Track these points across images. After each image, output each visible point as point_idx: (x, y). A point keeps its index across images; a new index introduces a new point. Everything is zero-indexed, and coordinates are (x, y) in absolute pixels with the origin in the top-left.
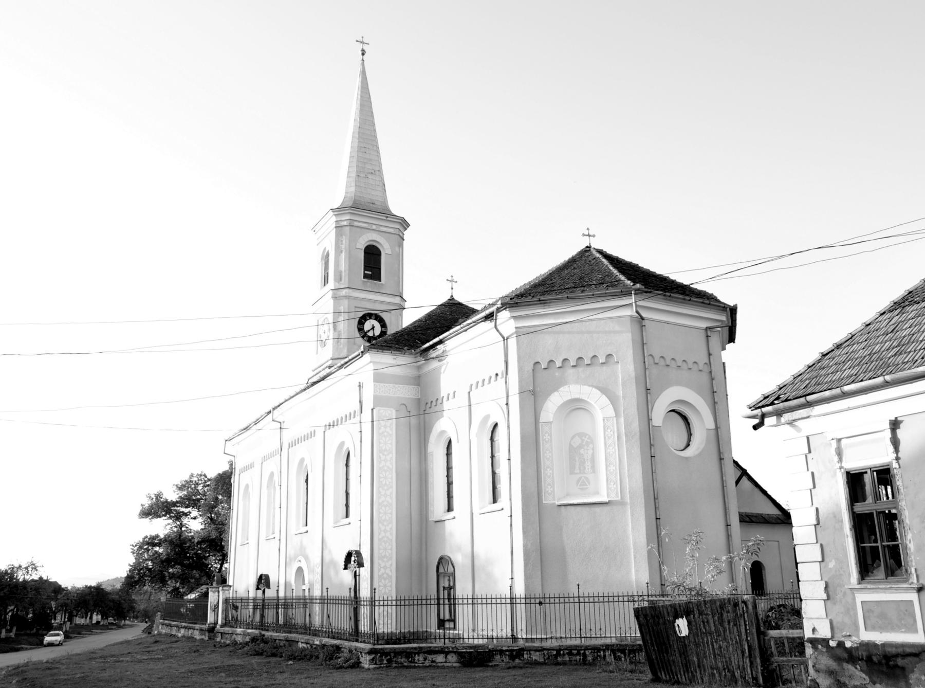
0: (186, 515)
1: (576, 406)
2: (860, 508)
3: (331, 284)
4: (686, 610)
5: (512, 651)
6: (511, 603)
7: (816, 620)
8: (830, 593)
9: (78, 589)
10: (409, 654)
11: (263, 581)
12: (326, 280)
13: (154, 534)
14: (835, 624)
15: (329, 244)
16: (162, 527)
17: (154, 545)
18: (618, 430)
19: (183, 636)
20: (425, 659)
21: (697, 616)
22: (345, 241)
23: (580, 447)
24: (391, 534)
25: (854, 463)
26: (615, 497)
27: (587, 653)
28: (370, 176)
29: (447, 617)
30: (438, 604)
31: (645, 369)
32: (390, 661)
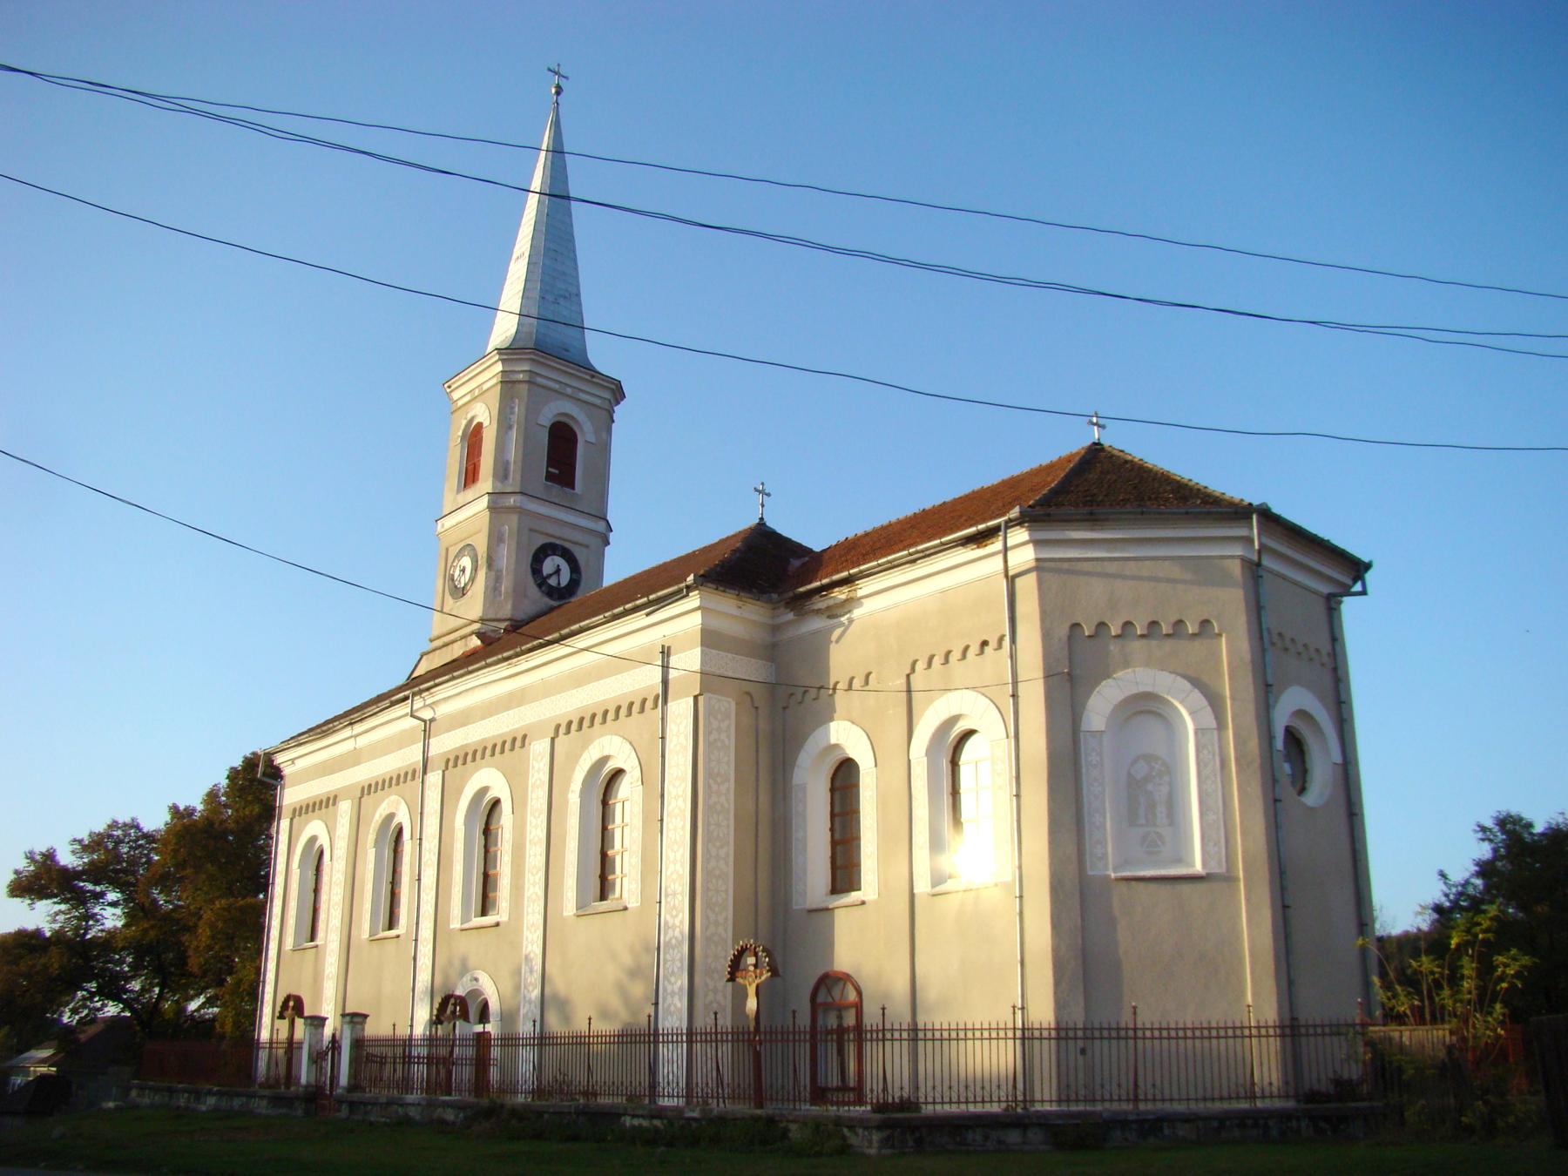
11: (451, 1007)
16: (42, 916)
20: (986, 1138)
22: (518, 409)
23: (1148, 778)
26: (1218, 868)
27: (1271, 1123)
28: (561, 301)
29: (834, 1081)
32: (919, 1142)
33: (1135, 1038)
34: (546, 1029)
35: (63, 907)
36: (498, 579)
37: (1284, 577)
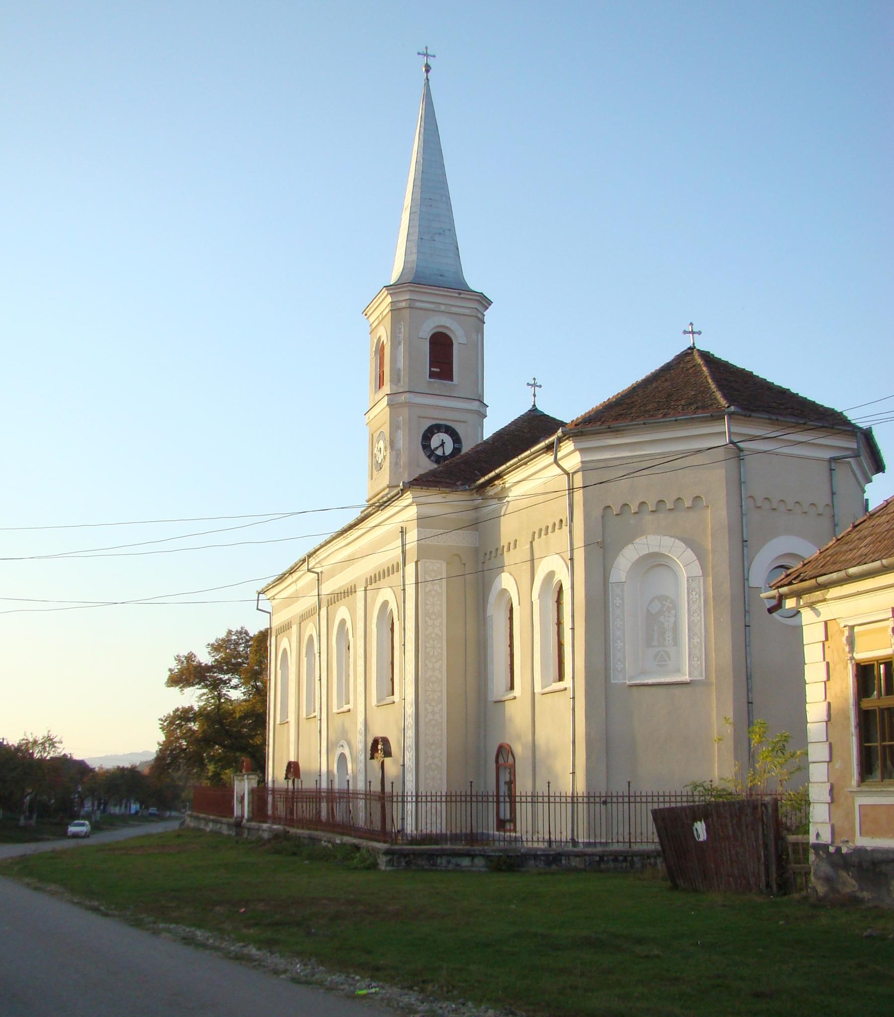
0: (225, 682)
1: (655, 562)
2: (867, 704)
3: (387, 389)
4: (703, 812)
5: (547, 856)
6: (573, 803)
7: (820, 826)
8: (835, 796)
9: (107, 771)
10: (432, 856)
11: (293, 769)
12: (381, 384)
13: (187, 706)
14: (836, 829)
15: (383, 333)
16: (193, 697)
17: (189, 720)
18: (705, 593)
19: (211, 831)
20: (449, 862)
21: (715, 818)
22: (403, 329)
24: (441, 717)
25: (863, 654)
26: (698, 676)
27: (635, 859)
28: (437, 238)
29: (508, 816)
30: (498, 802)
31: (742, 515)
32: (408, 863)
33: (488, 802)
34: (276, 786)
35: (205, 691)
36: (398, 456)
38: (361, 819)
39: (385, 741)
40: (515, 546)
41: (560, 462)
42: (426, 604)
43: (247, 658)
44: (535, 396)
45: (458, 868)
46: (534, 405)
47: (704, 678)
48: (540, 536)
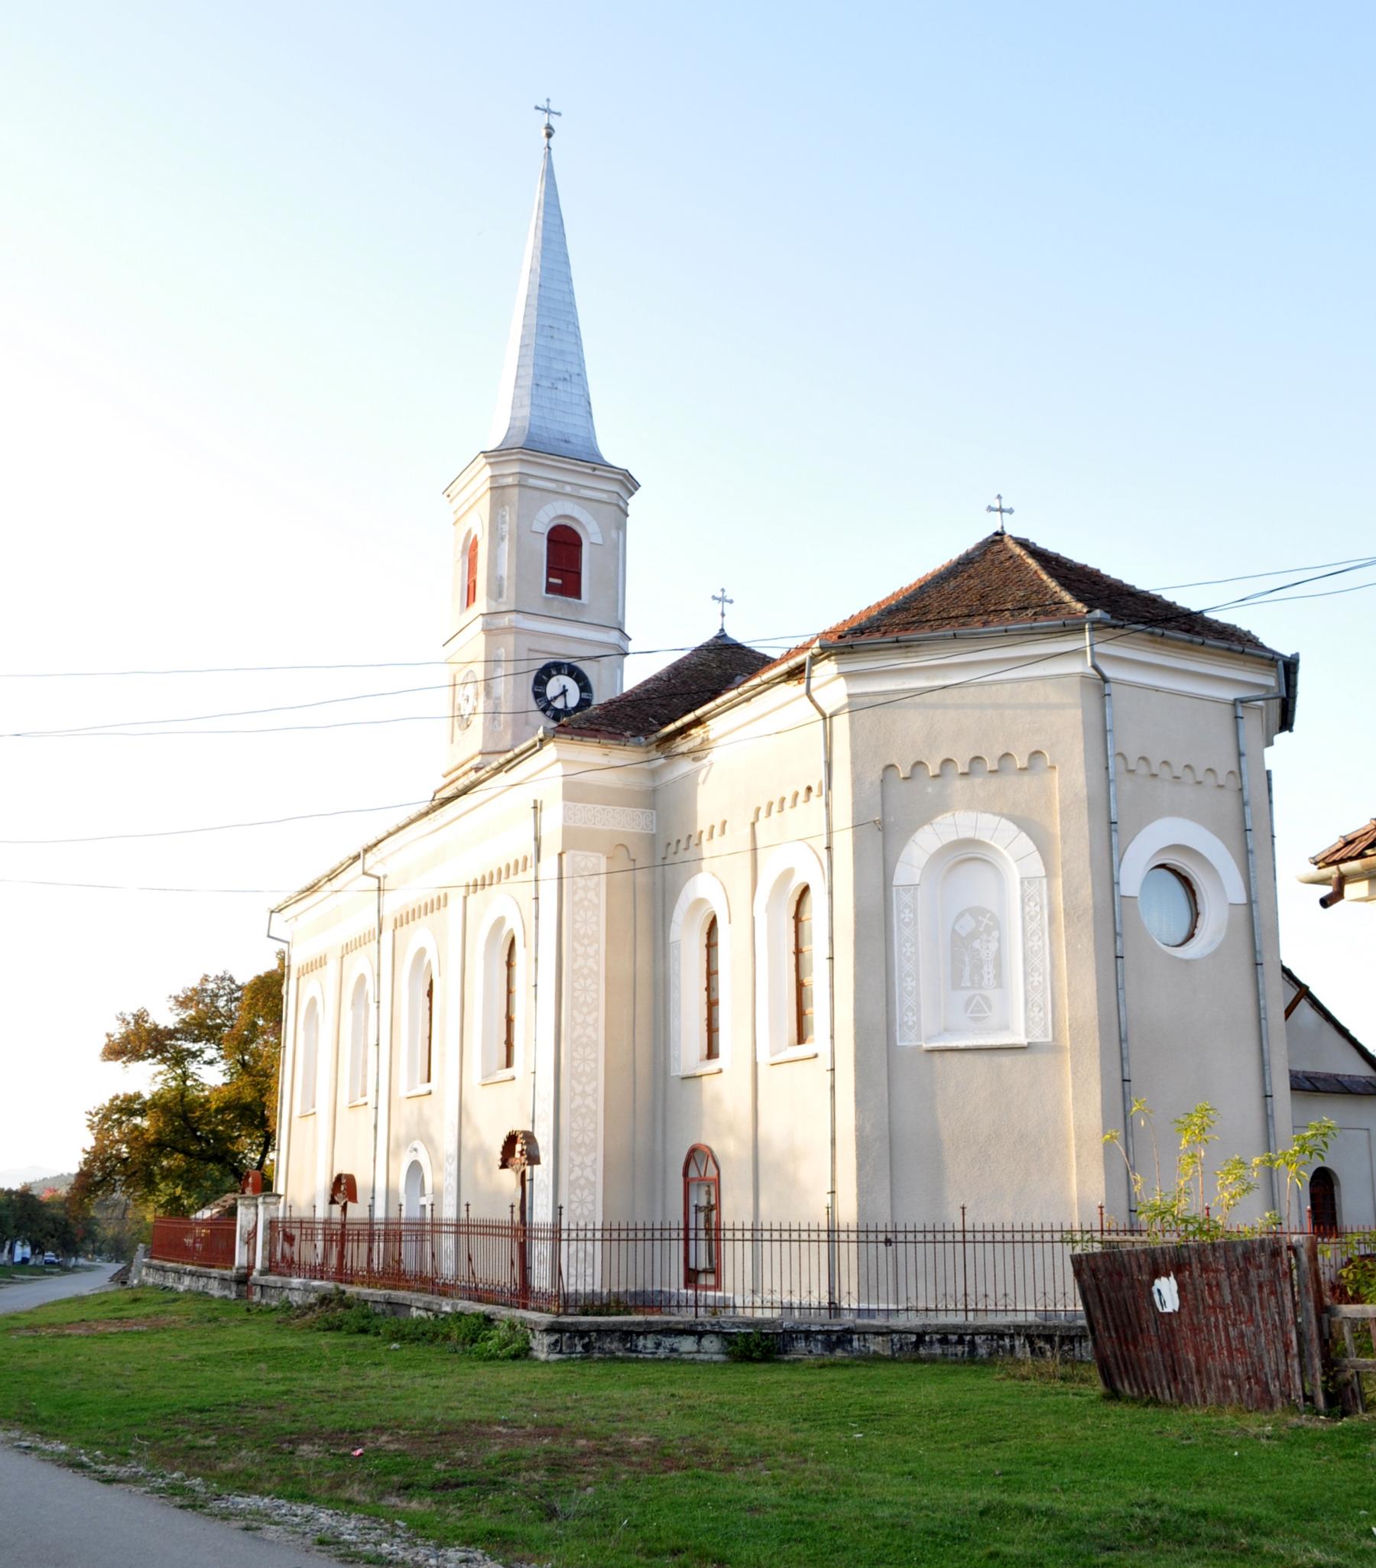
0: (194, 1055)
1: (966, 853)
3: (481, 604)
4: (1174, 1262)
5: (828, 1333)
11: (343, 1188)
15: (479, 523)
16: (146, 1078)
17: (133, 1113)
19: (188, 1291)
20: (658, 1345)
22: (509, 516)
23: (973, 935)
24: (596, 1101)
26: (1041, 1036)
27: (978, 1340)
28: (560, 385)
31: (1108, 782)
32: (587, 1347)
35: (163, 1067)
37: (1157, 690)
38: (448, 1268)
39: (529, 1137)
40: (723, 831)
41: (814, 695)
42: (575, 921)
43: (230, 1018)
44: (723, 615)
45: (675, 1355)
46: (722, 630)
47: (1050, 1039)
48: (769, 813)
